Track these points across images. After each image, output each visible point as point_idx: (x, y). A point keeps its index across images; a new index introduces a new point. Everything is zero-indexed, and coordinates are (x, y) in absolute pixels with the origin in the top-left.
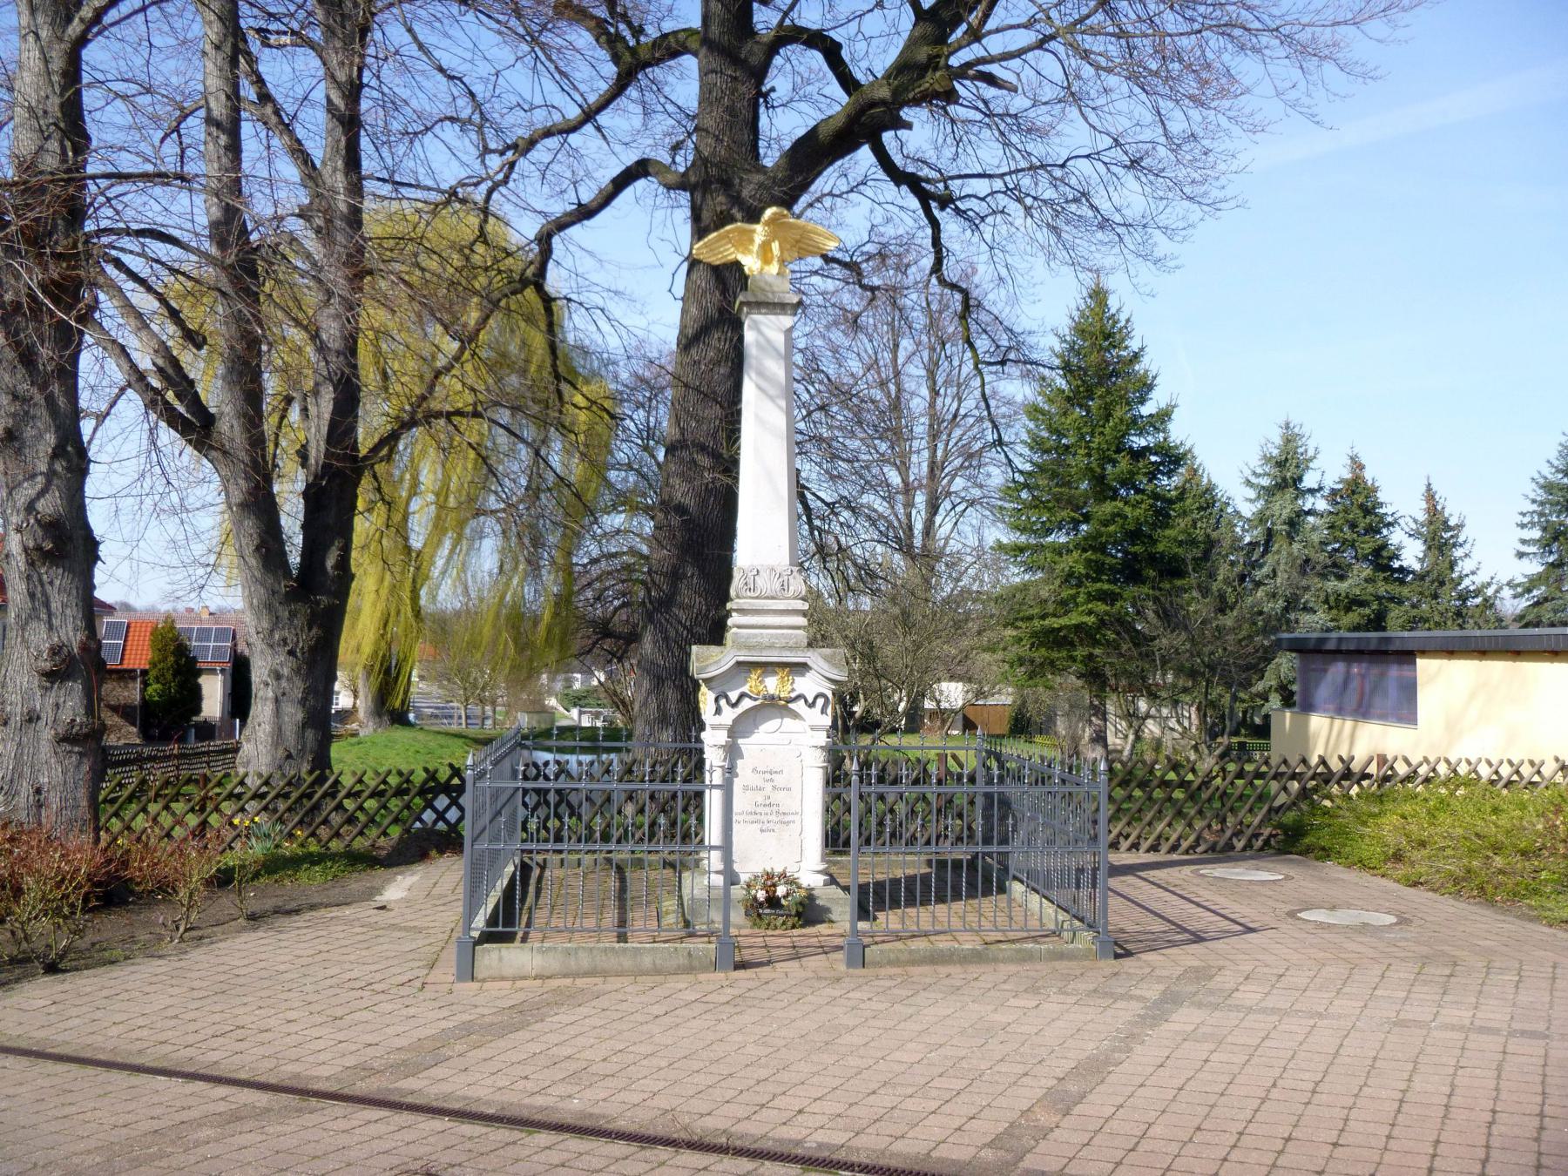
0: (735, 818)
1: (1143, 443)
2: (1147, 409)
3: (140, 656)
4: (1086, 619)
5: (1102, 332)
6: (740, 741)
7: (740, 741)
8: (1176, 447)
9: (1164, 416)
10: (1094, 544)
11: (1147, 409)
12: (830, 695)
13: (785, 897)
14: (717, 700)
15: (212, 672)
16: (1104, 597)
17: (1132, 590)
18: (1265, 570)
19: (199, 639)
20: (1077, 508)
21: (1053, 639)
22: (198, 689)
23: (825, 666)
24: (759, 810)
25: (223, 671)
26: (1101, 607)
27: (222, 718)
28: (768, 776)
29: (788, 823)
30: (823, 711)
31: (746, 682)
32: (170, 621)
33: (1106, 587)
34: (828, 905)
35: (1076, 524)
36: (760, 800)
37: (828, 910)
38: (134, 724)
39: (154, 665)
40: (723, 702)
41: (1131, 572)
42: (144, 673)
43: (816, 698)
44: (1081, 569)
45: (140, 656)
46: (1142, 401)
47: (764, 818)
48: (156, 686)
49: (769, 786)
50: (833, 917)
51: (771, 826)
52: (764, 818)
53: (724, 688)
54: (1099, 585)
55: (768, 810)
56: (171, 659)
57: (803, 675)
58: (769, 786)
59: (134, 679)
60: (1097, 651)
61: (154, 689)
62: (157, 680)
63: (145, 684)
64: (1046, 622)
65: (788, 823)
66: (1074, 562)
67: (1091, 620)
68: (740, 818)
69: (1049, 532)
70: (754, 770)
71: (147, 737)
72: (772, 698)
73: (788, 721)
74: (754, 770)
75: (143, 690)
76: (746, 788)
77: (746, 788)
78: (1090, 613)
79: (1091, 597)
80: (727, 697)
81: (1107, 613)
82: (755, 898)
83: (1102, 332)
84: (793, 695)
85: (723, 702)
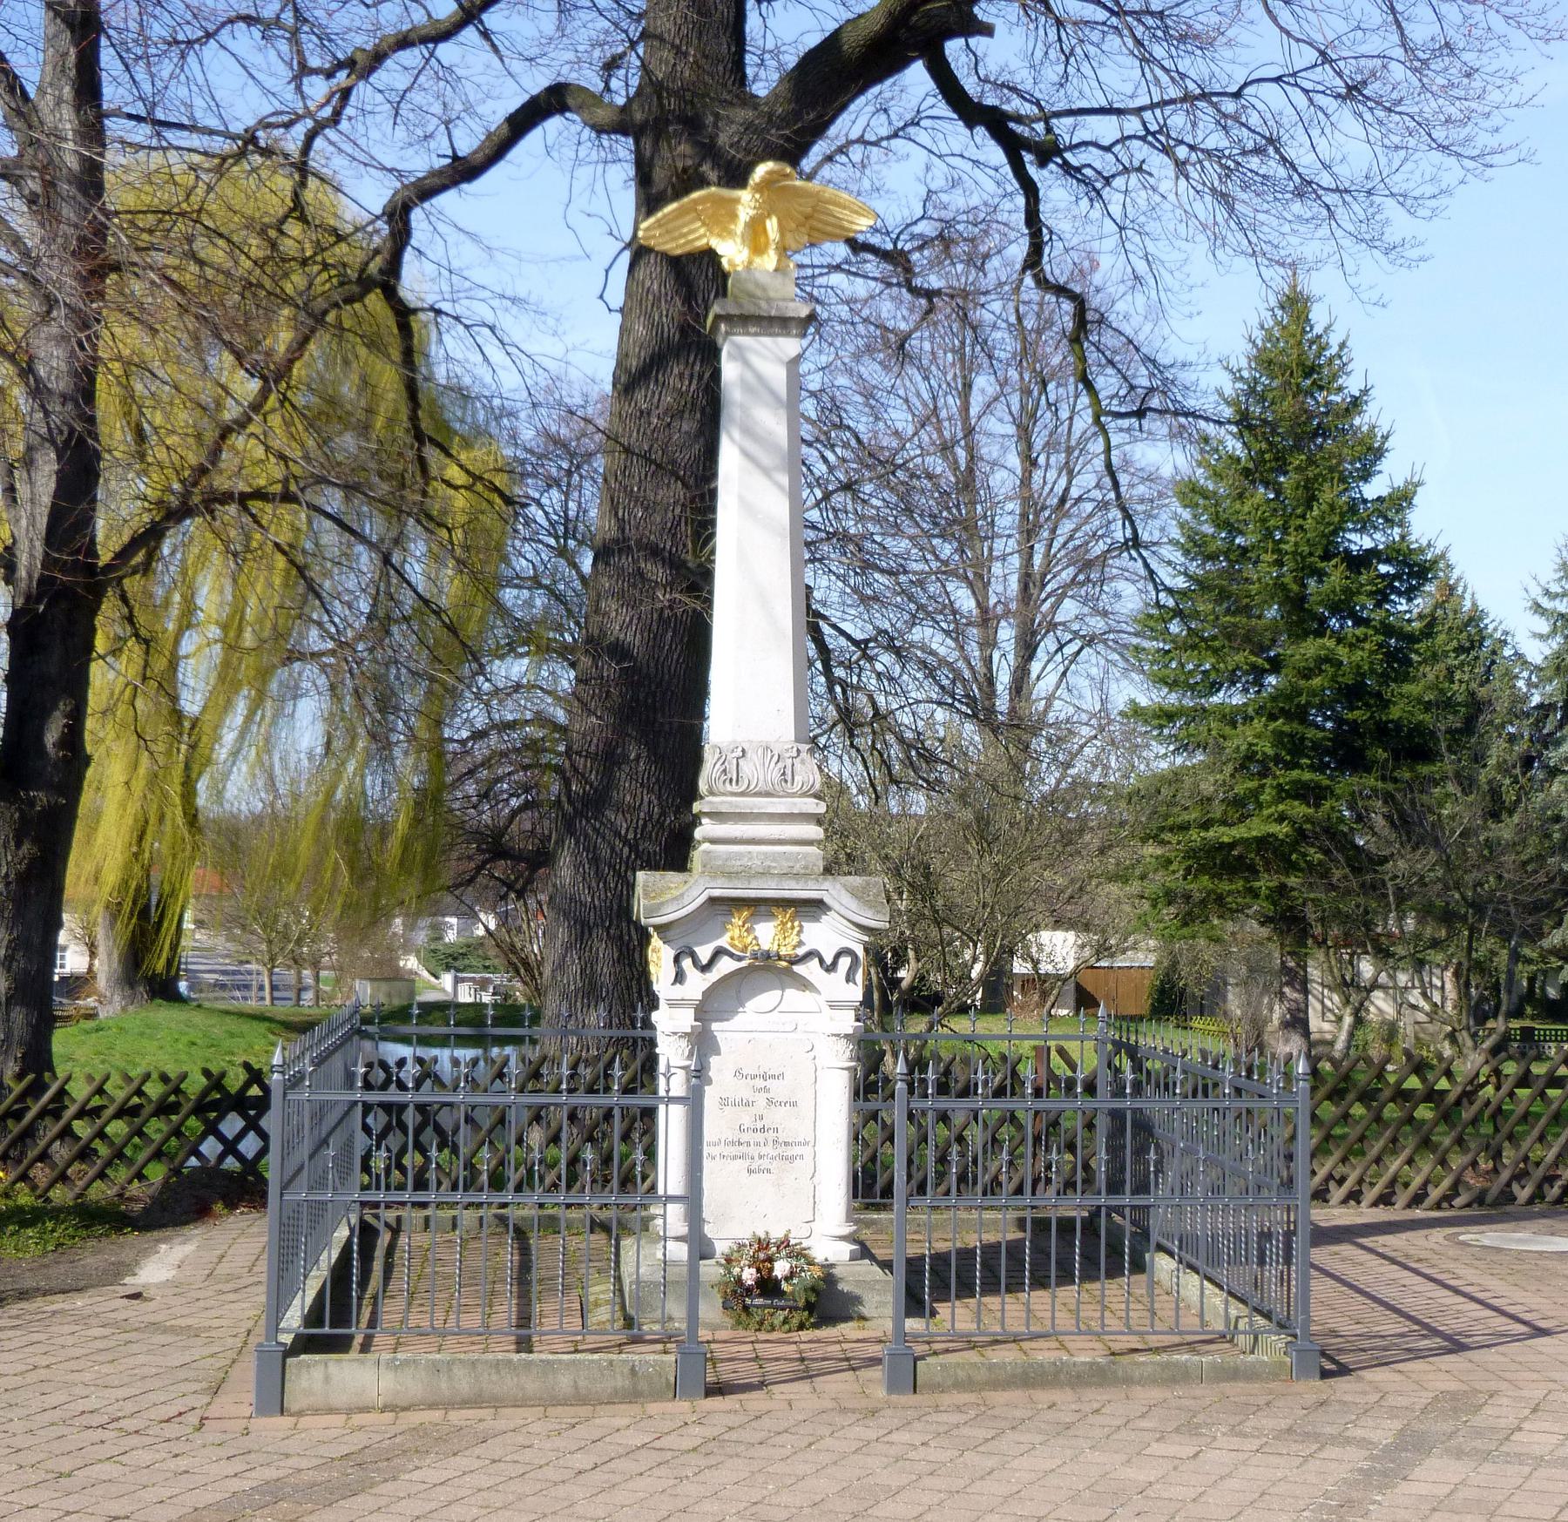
2: (1373, 489)
4: (1274, 828)
6: (715, 1026)
7: (715, 1026)
8: (1421, 550)
9: (1401, 500)
10: (1288, 707)
11: (1373, 489)
13: (788, 1279)
14: (677, 960)
16: (1302, 792)
17: (1349, 782)
20: (1260, 649)
23: (853, 904)
24: (745, 1137)
26: (1299, 809)
28: (760, 1083)
29: (792, 1159)
30: (849, 978)
31: (725, 930)
33: (1307, 776)
34: (857, 1291)
35: (1258, 674)
36: (747, 1122)
37: (857, 1300)
40: (687, 963)
46: (1366, 476)
49: (761, 1099)
50: (865, 1311)
51: (765, 1163)
55: (759, 1137)
58: (761, 1099)
65: (792, 1159)
66: (1255, 736)
67: (1282, 830)
68: (715, 1151)
72: (767, 956)
73: (792, 994)
74: (738, 1073)
76: (724, 1102)
77: (724, 1102)
78: (1281, 818)
79: (1283, 794)
80: (693, 955)
81: (1308, 819)
82: (739, 1281)
83: (1301, 364)
84: (801, 951)
85: (687, 963)
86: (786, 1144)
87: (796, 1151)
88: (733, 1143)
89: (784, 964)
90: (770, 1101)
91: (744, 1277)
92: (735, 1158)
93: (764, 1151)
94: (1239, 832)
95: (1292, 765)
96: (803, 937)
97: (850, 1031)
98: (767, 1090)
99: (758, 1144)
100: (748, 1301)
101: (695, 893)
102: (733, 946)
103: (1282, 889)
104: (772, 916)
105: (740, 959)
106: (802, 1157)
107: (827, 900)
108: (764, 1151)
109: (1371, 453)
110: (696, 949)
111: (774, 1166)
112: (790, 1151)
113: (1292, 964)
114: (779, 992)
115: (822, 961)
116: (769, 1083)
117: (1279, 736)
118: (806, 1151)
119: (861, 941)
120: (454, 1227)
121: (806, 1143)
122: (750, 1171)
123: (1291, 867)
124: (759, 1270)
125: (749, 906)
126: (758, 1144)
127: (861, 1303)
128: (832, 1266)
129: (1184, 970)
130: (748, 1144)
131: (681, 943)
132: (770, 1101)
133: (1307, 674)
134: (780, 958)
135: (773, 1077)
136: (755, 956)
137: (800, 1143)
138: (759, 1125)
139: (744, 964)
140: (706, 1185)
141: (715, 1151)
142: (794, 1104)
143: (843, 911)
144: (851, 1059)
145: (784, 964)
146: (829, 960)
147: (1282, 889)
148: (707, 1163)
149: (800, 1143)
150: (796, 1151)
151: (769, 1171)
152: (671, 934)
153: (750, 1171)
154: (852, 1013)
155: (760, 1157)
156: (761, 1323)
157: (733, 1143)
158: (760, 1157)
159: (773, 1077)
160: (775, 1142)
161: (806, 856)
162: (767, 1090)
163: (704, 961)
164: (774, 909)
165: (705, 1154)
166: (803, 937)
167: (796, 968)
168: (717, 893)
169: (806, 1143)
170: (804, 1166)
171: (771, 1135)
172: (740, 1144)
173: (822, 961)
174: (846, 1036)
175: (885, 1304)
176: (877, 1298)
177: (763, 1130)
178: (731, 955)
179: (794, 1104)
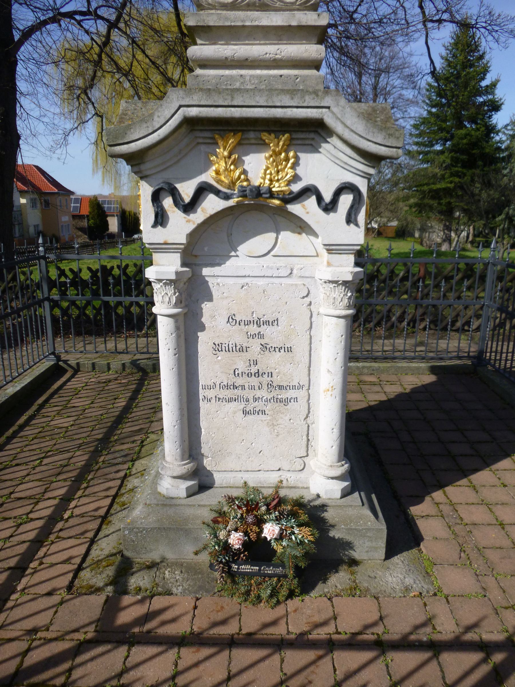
0: (202, 393)
1: (481, 100)
2: (484, 84)
3: (86, 210)
4: (449, 185)
5: (467, 44)
6: (206, 271)
7: (206, 271)
8: (498, 101)
9: (494, 85)
10: (454, 149)
11: (484, 84)
12: (364, 189)
13: (280, 537)
14: (156, 198)
15: (113, 216)
16: (456, 174)
17: (469, 172)
18: (508, 170)
19: (108, 204)
20: (448, 132)
21: (436, 195)
22: (107, 221)
23: (360, 126)
24: (239, 381)
25: (117, 216)
26: (457, 180)
27: (118, 233)
28: (253, 329)
29: (286, 401)
30: (351, 219)
31: (209, 164)
32: (95, 198)
33: (460, 169)
34: (348, 538)
35: (446, 140)
36: (241, 366)
37: (349, 545)
38: (86, 234)
39: (90, 213)
40: (168, 202)
41: (470, 164)
42: (88, 216)
43: (338, 193)
44: (448, 161)
45: (86, 210)
46: (483, 79)
47: (248, 394)
48: (92, 221)
49: (255, 345)
50: (356, 555)
51: (259, 405)
52: (248, 394)
53: (167, 175)
54: (456, 169)
55: (254, 381)
56: (96, 211)
57: (315, 149)
58: (255, 345)
59: (84, 218)
60: (452, 201)
61: (91, 221)
62: (92, 218)
63: (88, 220)
64: (430, 187)
65: (286, 401)
66: (446, 159)
67: (452, 186)
68: (210, 394)
69: (433, 145)
70: (231, 319)
71: (90, 238)
72: (257, 192)
73: (286, 236)
74: (231, 319)
75: (88, 222)
76: (218, 348)
77: (218, 348)
78: (451, 182)
79: (452, 175)
80: (174, 193)
81: (459, 182)
82: (226, 547)
83: (467, 44)
84: (296, 188)
85: (168, 202)
86: (280, 387)
87: (291, 394)
88: (227, 387)
89: (277, 202)
90: (264, 347)
91: (230, 541)
92: (230, 400)
93: (259, 394)
94: (438, 186)
95: (456, 166)
96: (299, 171)
97: (350, 278)
98: (260, 336)
99: (252, 388)
100: (235, 567)
101: (168, 113)
102: (219, 181)
103: (450, 203)
104: (262, 145)
105: (227, 197)
106: (296, 399)
107: (329, 120)
108: (259, 394)
109: (485, 71)
110: (178, 186)
111: (268, 408)
112: (284, 395)
113: (448, 224)
114: (273, 235)
115: (320, 199)
116: (264, 329)
117: (452, 158)
118: (301, 394)
119: (368, 177)
120: (109, 369)
121: (300, 387)
122: (245, 413)
123: (451, 196)
124: (246, 534)
125: (235, 132)
126: (252, 388)
127: (352, 548)
128: (323, 507)
129: (410, 226)
130: (243, 387)
131: (159, 181)
132: (264, 347)
133: (462, 139)
134: (272, 195)
135: (267, 323)
136: (243, 193)
137: (294, 387)
138: (254, 370)
139: (231, 202)
140: (203, 424)
141: (210, 394)
142: (289, 350)
143: (347, 135)
144: (349, 307)
145: (277, 202)
146: (327, 197)
147: (450, 203)
148: (203, 406)
149: (294, 387)
150: (291, 394)
151: (264, 412)
152: (147, 167)
153: (245, 413)
154: (351, 258)
155: (255, 400)
156: (248, 593)
157: (227, 387)
158: (255, 400)
159: (267, 323)
160: (270, 385)
161: (305, 79)
162: (260, 336)
163: (187, 198)
164: (265, 136)
165: (201, 397)
166: (299, 171)
167: (294, 208)
168: (193, 112)
169: (300, 387)
170: (301, 407)
171: (265, 379)
172: (235, 387)
173: (320, 199)
174: (345, 283)
175: (376, 549)
176: (368, 544)
177: (258, 374)
178: (217, 193)
179: (289, 350)
